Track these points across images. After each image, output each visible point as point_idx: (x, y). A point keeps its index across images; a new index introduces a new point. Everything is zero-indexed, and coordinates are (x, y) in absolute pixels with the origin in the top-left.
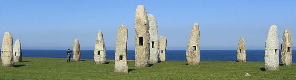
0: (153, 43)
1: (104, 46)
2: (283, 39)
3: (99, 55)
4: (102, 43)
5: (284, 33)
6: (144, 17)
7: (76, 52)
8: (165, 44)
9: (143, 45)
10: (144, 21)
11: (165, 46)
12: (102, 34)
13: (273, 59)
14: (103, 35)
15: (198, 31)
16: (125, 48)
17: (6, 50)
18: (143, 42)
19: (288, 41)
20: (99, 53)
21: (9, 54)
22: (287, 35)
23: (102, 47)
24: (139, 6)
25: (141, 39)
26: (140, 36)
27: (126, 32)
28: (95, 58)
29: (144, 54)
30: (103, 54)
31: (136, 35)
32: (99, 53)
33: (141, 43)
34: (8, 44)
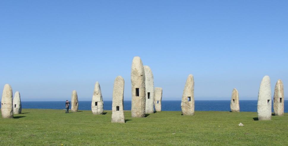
0: (149, 94)
1: (101, 97)
3: (96, 106)
7: (75, 103)
10: (140, 72)
14: (100, 86)
15: (193, 82)
16: (122, 99)
17: (6, 103)
19: (280, 92)
20: (96, 104)
23: (100, 98)
25: (137, 90)
27: (123, 83)
28: (92, 109)
29: (140, 104)
31: (132, 86)
32: (96, 104)
33: (137, 94)
34: (8, 97)
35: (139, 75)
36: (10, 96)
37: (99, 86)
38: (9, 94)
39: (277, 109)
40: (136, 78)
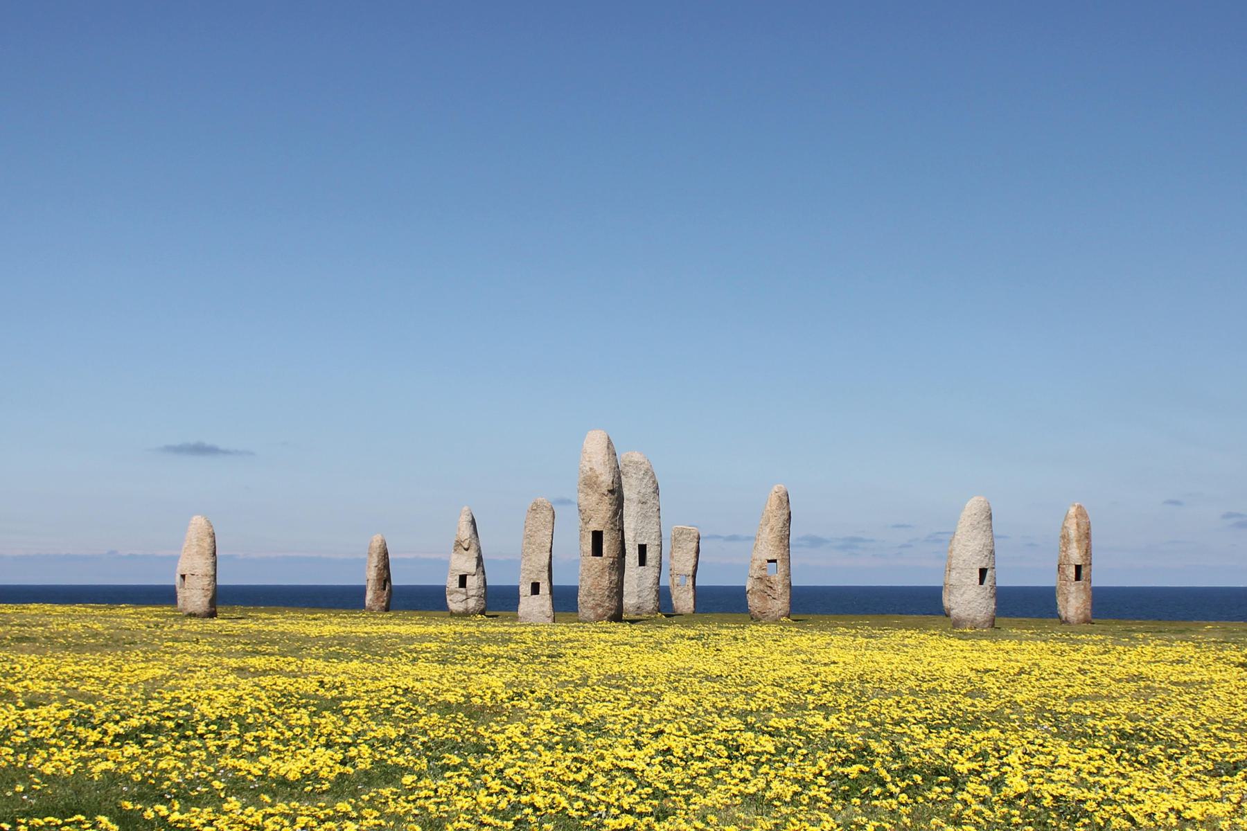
0: (642, 549)
1: (480, 560)
2: (1063, 537)
3: (463, 590)
4: (474, 547)
5: (1066, 519)
6: (608, 469)
7: (378, 580)
8: (693, 554)
9: (601, 555)
10: (606, 479)
11: (692, 562)
12: (473, 522)
13: (974, 595)
14: (192, 440)
15: (786, 512)
16: (547, 561)
17: (199, 572)
18: (604, 547)
19: (1075, 545)
20: (463, 581)
21: (206, 581)
22: (1075, 527)
23: (475, 563)
24: (591, 434)
25: (597, 537)
26: (594, 526)
27: (549, 518)
28: (448, 598)
29: (605, 583)
30: (476, 585)
31: (581, 523)
32: (463, 581)
33: (597, 551)
34: (203, 554)
35: (605, 490)
36: (208, 553)
37: (473, 522)
38: (206, 545)
39: (1067, 600)
40: (595, 498)
